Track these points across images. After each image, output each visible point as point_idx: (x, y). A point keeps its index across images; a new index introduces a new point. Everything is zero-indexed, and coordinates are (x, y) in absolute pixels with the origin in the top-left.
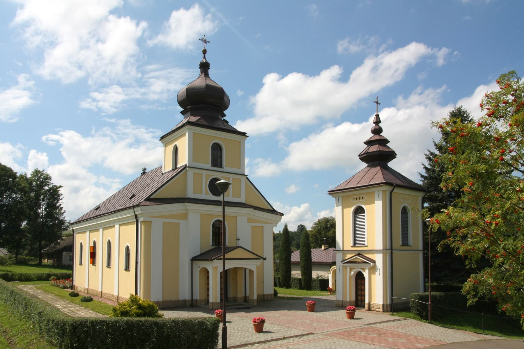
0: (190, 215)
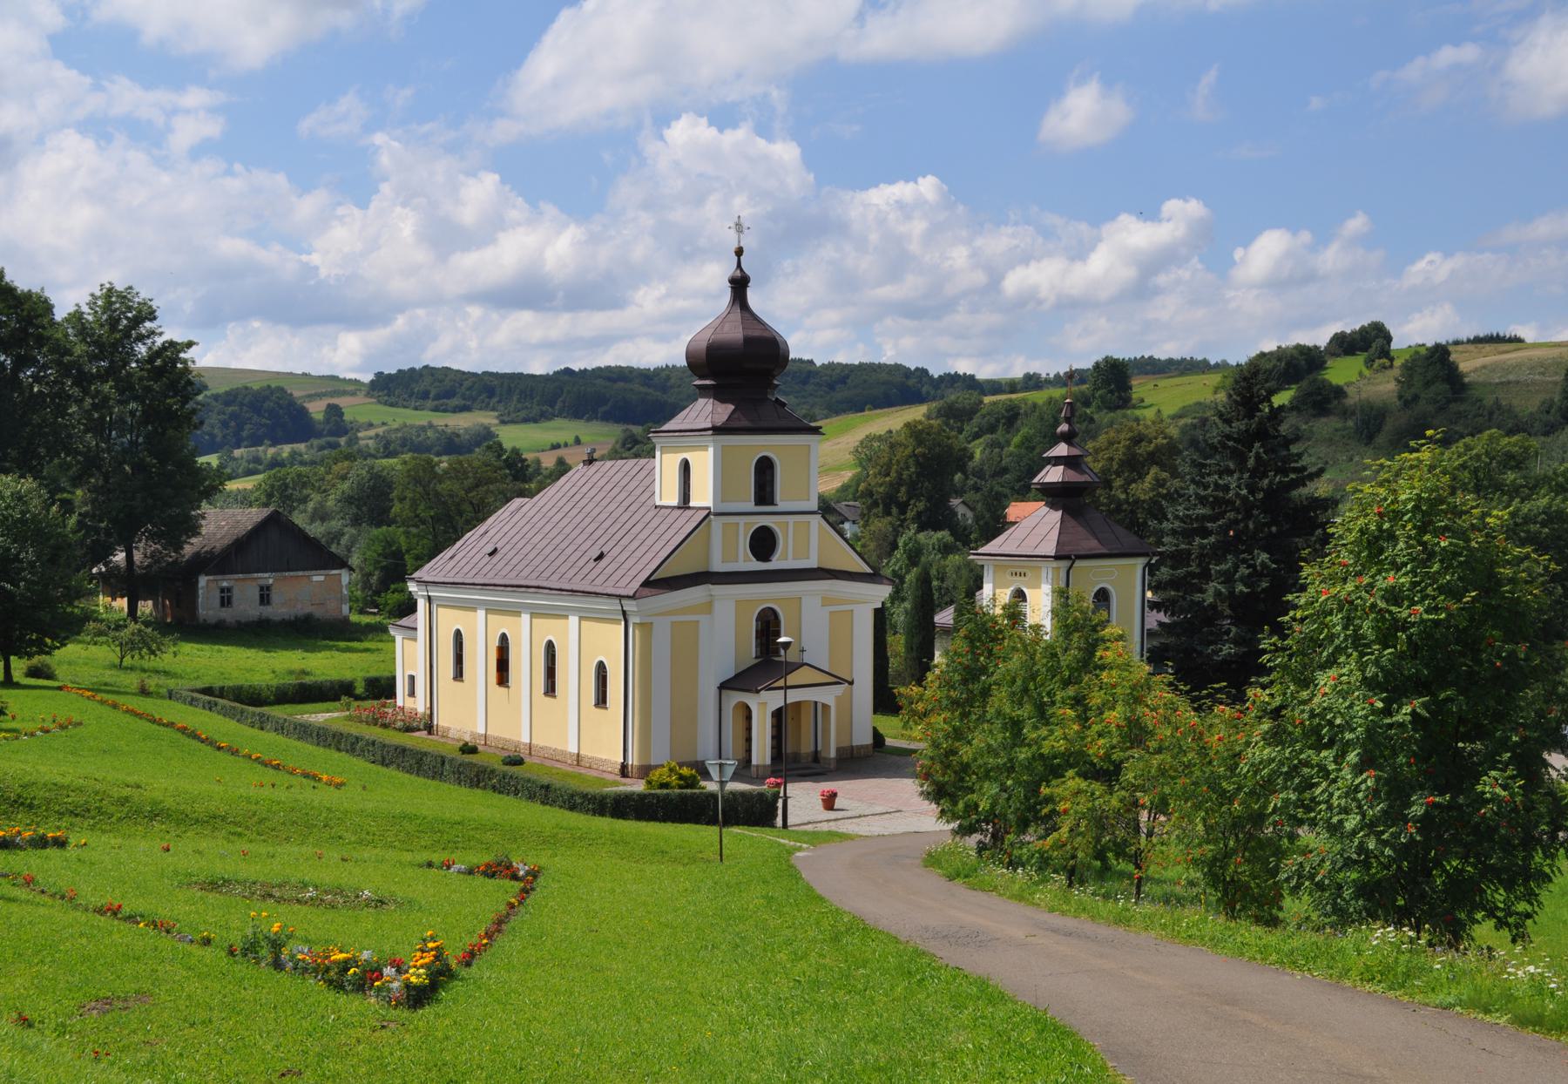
0: (717, 606)
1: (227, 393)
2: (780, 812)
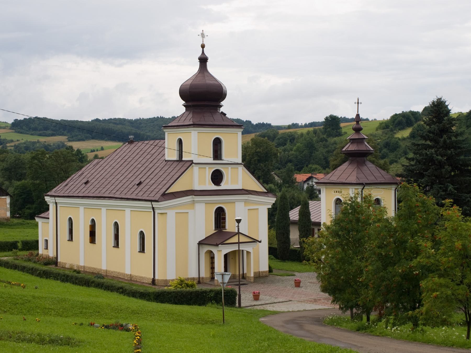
2: (237, 302)
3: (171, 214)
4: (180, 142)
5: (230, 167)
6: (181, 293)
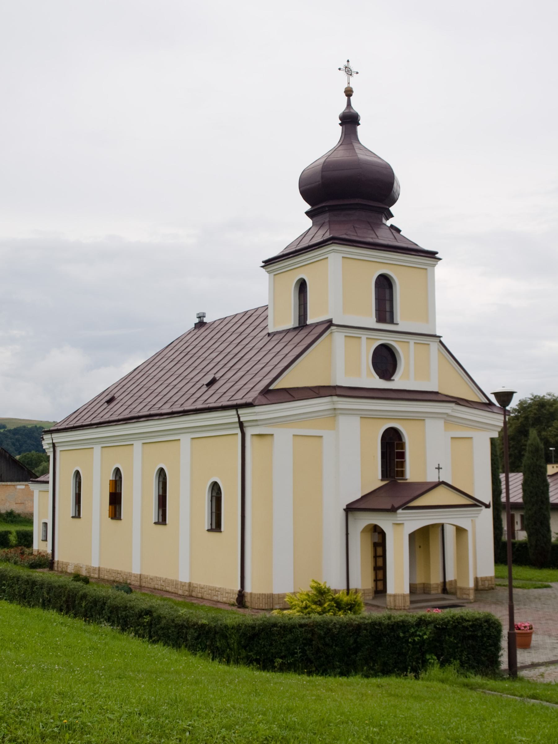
1: (15, 429)
3: (283, 437)
4: (302, 286)
5: (412, 340)
6: (324, 626)
